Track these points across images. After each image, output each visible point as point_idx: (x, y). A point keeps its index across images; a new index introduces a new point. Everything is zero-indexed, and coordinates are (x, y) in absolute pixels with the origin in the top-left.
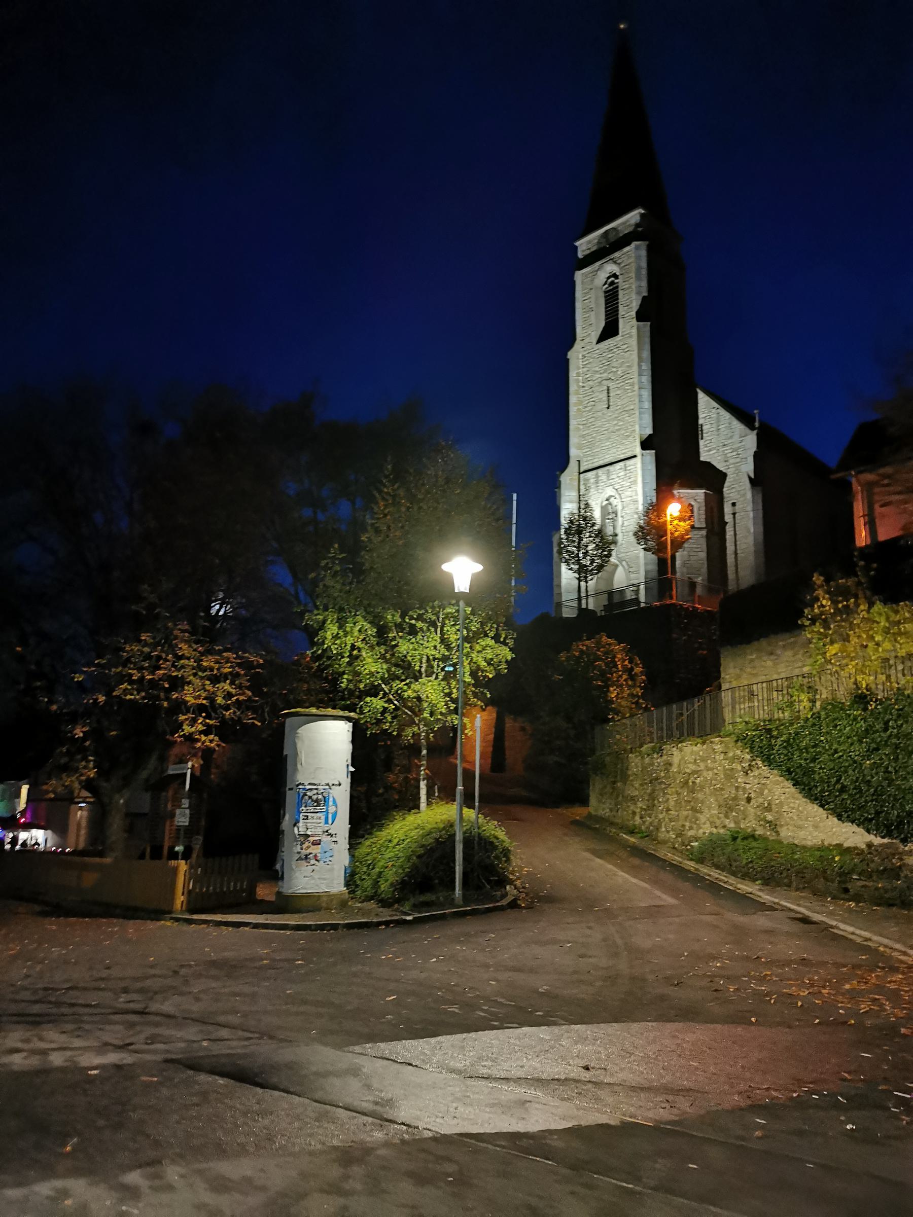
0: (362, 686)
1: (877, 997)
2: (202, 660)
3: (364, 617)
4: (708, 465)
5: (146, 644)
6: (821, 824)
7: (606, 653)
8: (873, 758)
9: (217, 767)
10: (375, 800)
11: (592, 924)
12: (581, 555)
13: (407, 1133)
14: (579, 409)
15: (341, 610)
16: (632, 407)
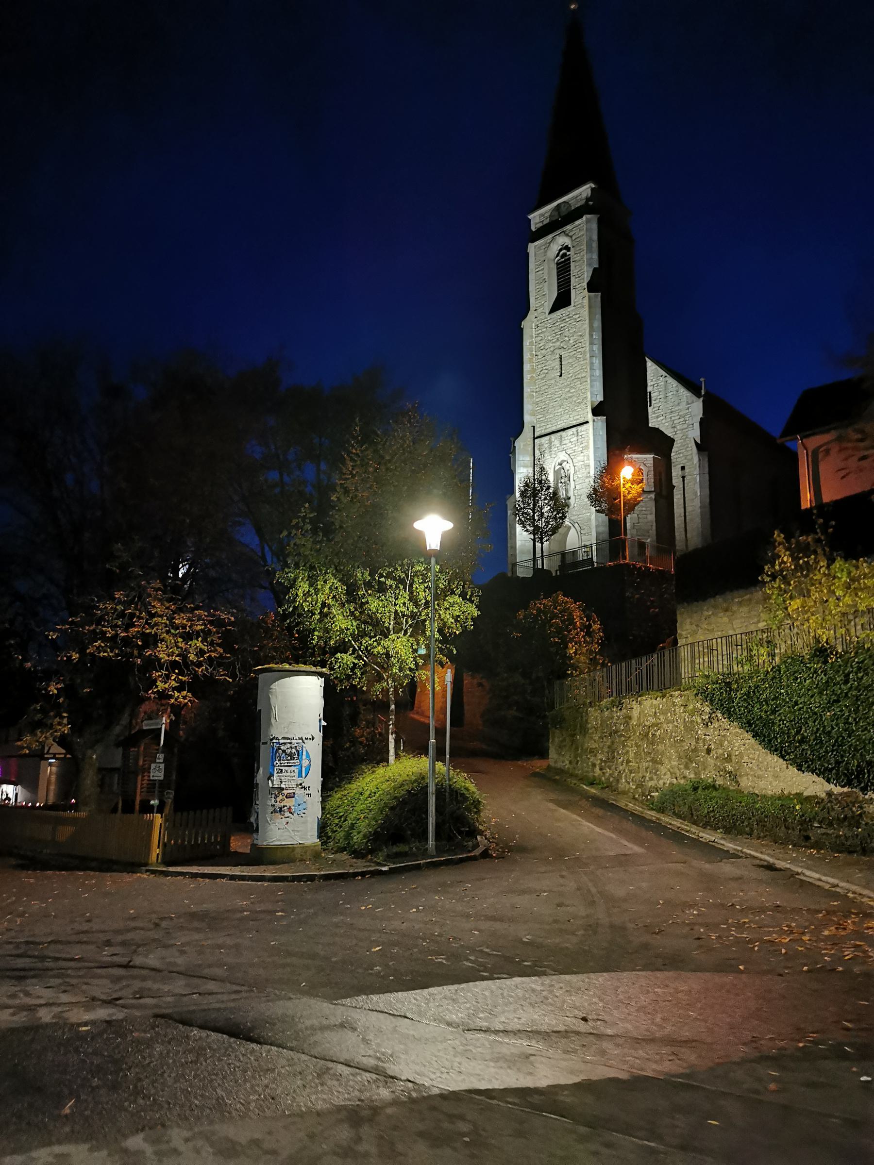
0: (332, 642)
1: (858, 943)
2: (174, 618)
3: (334, 575)
4: (657, 430)
5: (120, 602)
7: (564, 611)
8: (834, 710)
9: (185, 723)
10: (341, 754)
11: (564, 873)
12: (536, 518)
13: (414, 1090)
15: (312, 568)
16: (583, 375)
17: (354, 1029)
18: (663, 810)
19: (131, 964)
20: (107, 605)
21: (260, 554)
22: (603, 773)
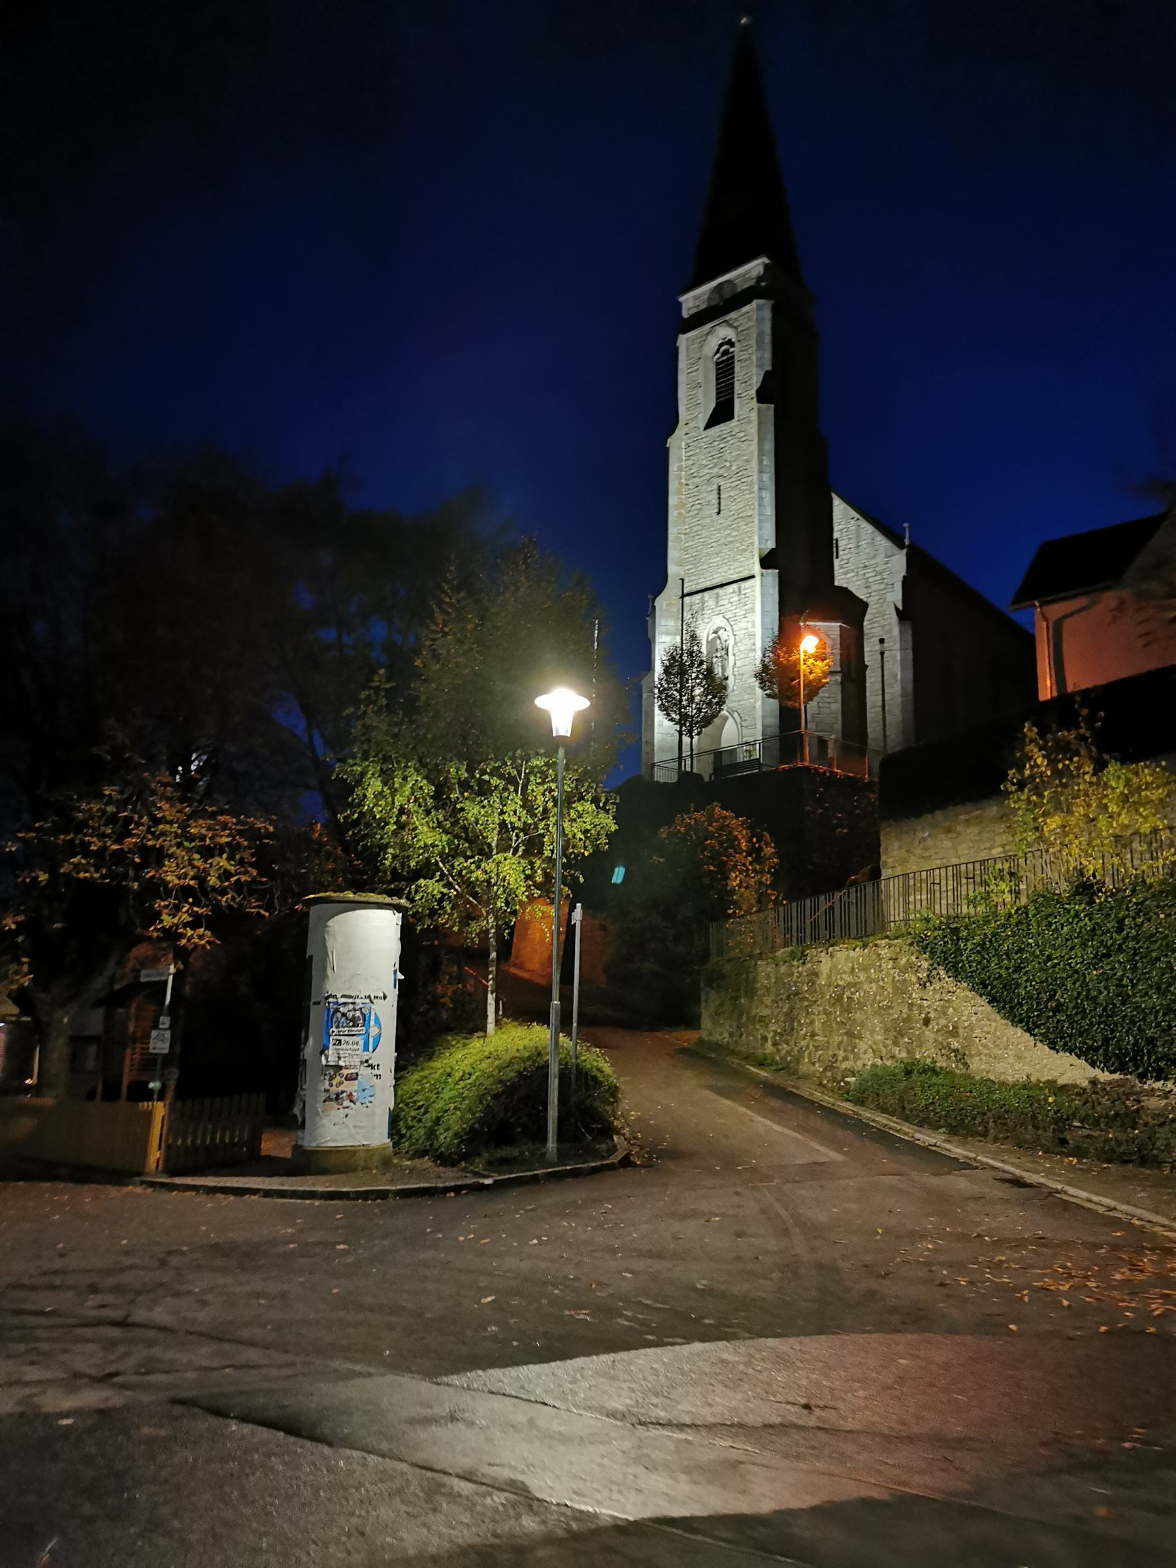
0: (413, 864)
2: (189, 826)
3: (417, 770)
4: (845, 591)
5: (110, 801)
6: (1026, 1054)
8: (1102, 967)
11: (739, 1189)
14: (680, 514)
16: (749, 514)
17: (471, 1424)
18: (863, 1101)
19: (130, 1320)
20: (92, 806)
21: (306, 741)
22: (778, 1050)
